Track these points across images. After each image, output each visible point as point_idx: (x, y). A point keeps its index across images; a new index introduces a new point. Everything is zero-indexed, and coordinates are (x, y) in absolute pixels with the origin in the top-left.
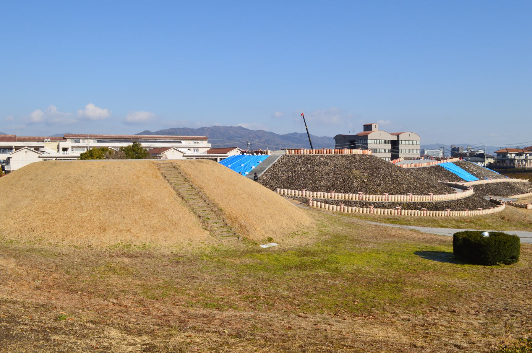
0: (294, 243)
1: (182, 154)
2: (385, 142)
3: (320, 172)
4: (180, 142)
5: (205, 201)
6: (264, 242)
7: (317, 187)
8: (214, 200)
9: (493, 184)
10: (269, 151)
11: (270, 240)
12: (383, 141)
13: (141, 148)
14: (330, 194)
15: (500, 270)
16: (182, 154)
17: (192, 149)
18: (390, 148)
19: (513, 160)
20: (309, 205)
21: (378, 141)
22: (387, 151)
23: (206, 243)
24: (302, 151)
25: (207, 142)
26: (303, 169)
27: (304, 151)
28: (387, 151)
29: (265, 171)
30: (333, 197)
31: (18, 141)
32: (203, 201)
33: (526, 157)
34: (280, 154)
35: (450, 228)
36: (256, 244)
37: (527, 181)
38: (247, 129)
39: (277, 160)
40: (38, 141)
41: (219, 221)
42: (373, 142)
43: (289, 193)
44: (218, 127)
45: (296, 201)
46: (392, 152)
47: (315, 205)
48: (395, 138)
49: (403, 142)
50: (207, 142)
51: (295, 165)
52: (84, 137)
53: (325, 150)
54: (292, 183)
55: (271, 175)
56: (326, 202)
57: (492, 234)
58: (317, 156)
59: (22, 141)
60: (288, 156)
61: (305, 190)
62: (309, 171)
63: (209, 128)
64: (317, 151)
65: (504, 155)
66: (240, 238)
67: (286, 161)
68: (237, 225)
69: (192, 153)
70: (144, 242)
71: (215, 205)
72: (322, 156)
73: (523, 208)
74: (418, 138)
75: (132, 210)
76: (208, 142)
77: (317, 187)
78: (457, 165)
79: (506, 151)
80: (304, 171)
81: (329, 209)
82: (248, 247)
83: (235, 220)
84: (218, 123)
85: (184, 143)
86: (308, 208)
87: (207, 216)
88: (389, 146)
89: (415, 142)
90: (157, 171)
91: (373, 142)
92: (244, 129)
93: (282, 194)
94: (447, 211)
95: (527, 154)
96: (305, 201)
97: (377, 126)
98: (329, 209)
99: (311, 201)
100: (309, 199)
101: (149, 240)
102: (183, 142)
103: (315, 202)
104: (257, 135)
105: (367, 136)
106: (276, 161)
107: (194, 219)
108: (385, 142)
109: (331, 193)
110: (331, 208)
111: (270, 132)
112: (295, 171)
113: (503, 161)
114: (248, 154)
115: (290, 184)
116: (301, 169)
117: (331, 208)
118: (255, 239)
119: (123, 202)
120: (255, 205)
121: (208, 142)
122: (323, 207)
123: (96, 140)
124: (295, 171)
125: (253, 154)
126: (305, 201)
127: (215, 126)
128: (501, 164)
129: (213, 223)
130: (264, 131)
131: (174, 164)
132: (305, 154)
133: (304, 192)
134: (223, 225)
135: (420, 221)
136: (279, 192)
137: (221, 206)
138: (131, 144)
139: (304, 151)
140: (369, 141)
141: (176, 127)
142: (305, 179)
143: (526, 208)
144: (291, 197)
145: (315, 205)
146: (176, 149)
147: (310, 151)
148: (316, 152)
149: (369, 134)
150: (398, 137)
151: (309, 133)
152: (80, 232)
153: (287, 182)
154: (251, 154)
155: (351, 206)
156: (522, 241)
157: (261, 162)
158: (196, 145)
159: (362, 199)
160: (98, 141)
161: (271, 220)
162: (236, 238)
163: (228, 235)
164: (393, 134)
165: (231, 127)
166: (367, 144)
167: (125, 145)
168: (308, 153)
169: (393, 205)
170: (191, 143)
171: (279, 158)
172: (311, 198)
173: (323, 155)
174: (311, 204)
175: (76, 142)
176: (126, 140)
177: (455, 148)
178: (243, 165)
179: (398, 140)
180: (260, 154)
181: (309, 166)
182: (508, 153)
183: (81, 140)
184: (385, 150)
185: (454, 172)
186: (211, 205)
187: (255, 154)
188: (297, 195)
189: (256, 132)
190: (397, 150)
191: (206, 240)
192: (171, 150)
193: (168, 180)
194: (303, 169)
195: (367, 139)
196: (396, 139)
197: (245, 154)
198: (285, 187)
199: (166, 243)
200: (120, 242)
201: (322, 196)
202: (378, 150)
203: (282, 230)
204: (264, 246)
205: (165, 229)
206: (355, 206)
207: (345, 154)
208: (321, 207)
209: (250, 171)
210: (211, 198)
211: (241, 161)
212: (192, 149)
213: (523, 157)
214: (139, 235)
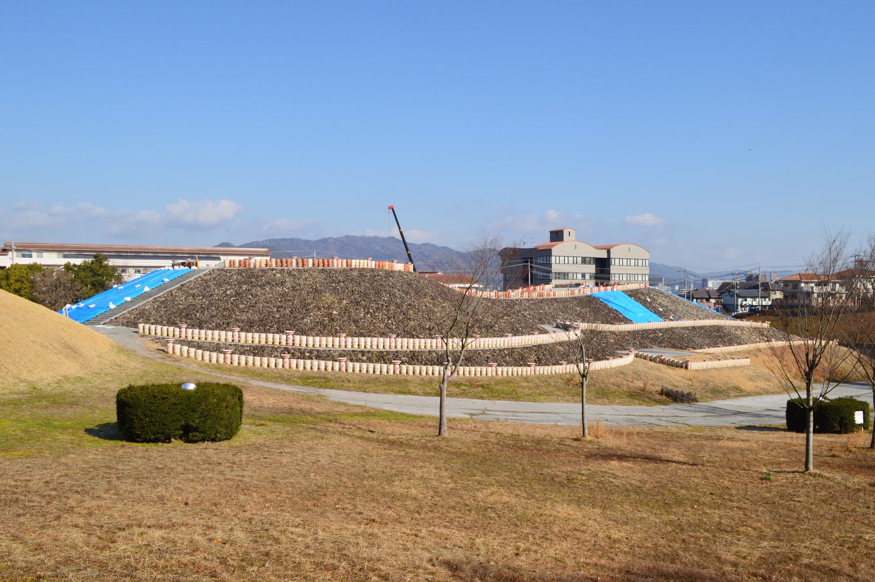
2: (584, 261)
9: (684, 328)
12: (580, 260)
13: (106, 266)
15: (208, 449)
18: (594, 271)
19: (809, 294)
21: (571, 259)
22: (587, 277)
26: (228, 292)
28: (587, 277)
30: (343, 344)
33: (833, 289)
35: (418, 394)
37: (766, 325)
42: (562, 262)
44: (354, 237)
46: (596, 278)
48: (603, 254)
49: (617, 260)
52: (43, 249)
53: (294, 261)
57: (198, 385)
63: (337, 239)
64: (279, 261)
65: (796, 284)
73: (681, 367)
74: (646, 255)
78: (630, 296)
79: (797, 278)
80: (227, 295)
84: (357, 233)
88: (592, 269)
89: (640, 261)
91: (562, 262)
94: (491, 366)
95: (835, 283)
97: (573, 233)
103: (178, 347)
104: (421, 252)
105: (550, 250)
108: (584, 261)
113: (794, 296)
122: (192, 354)
128: (790, 302)
130: (434, 246)
135: (366, 384)
136: (141, 331)
138: (90, 260)
140: (553, 258)
141: (279, 237)
143: (686, 368)
148: (297, 263)
149: (553, 246)
150: (609, 252)
151: (407, 240)
155: (304, 358)
156: (247, 397)
164: (597, 248)
165: (376, 238)
166: (550, 265)
167: (78, 262)
169: (382, 357)
175: (24, 256)
176: (79, 252)
177: (751, 276)
179: (609, 258)
182: (800, 282)
183: (34, 254)
184: (583, 276)
185: (615, 307)
190: (606, 276)
194: (228, 292)
195: (550, 255)
196: (606, 257)
202: (570, 276)
206: (310, 358)
207: (335, 267)
213: (829, 288)
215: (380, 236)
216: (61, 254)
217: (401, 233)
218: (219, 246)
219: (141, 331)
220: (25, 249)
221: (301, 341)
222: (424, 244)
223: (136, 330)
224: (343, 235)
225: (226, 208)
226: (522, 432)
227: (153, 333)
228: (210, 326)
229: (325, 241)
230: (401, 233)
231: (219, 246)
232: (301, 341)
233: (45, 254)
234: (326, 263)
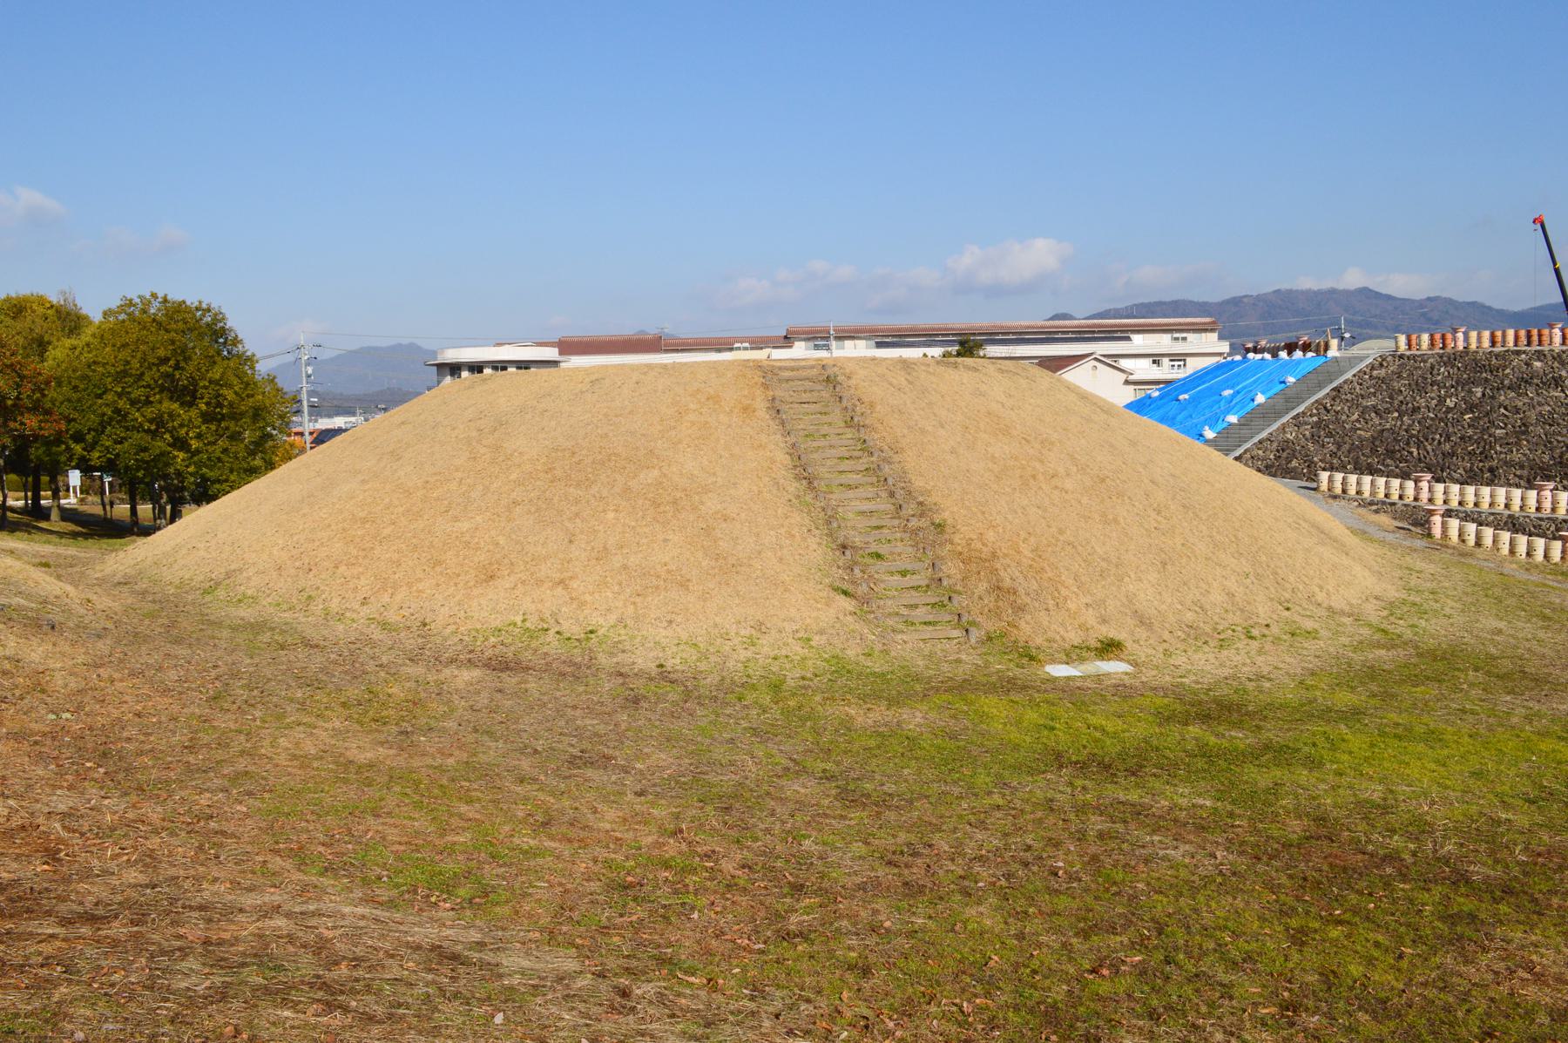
0: (1204, 667)
1: (1123, 377)
3: (1517, 410)
4: (1128, 339)
5: (892, 495)
6: (1072, 655)
7: (1491, 470)
8: (928, 493)
10: (1334, 343)
11: (1109, 648)
14: (1533, 494)
16: (1123, 377)
17: (1166, 361)
20: (1430, 535)
23: (817, 640)
24: (1460, 336)
25: (1215, 335)
26: (1450, 403)
27: (1466, 338)
29: (1301, 409)
30: (1547, 505)
31: (667, 351)
32: (884, 495)
34: (1371, 350)
36: (1032, 658)
38: (1389, 297)
39: (1355, 371)
40: (719, 351)
41: (917, 566)
43: (1366, 489)
45: (1384, 519)
47: (1454, 533)
50: (1215, 335)
51: (1419, 388)
54: (1390, 453)
55: (1317, 425)
56: (1514, 524)
58: (1518, 353)
59: (677, 351)
60: (1401, 357)
61: (1551, 485)
62: (1471, 409)
64: (1523, 333)
66: (975, 634)
67: (1380, 378)
68: (983, 586)
69: (1165, 371)
70: (596, 620)
71: (923, 510)
72: (1540, 355)
75: (611, 515)
76: (1221, 338)
77: (1491, 470)
80: (1449, 410)
81: (1512, 552)
82: (987, 664)
83: (980, 562)
85: (1139, 342)
86: (1420, 543)
87: (874, 548)
90: (759, 392)
92: (1378, 295)
93: (1338, 490)
96: (1417, 520)
98: (1512, 552)
99: (1437, 519)
100: (1431, 513)
101: (612, 619)
102: (1137, 339)
104: (1423, 315)
106: (1349, 375)
107: (817, 550)
109: (1540, 489)
110: (1522, 549)
111: (1473, 304)
112: (1416, 410)
114: (1259, 356)
115: (1384, 454)
116: (1441, 401)
117: (1522, 549)
118: (1039, 641)
119: (594, 490)
120: (1104, 515)
121: (1221, 338)
122: (1488, 541)
123: (872, 343)
124: (1416, 410)
125: (1275, 355)
126: (1417, 520)
127: (1278, 292)
129: (892, 574)
130: (1450, 301)
131: (830, 372)
132: (1473, 346)
133: (1547, 494)
134: (924, 583)
136: (1324, 486)
137: (946, 515)
139: (1466, 338)
142: (1448, 439)
144: (1371, 504)
145: (1454, 533)
146: (1111, 361)
147: (1493, 336)
152: (420, 580)
153: (1374, 451)
154: (1267, 356)
157: (1291, 380)
158: (1180, 348)
159: (1554, 510)
160: (880, 345)
161: (1153, 576)
162: (956, 633)
163: (930, 618)
165: (1333, 291)
168: (1486, 343)
170: (1163, 343)
171: (1362, 365)
172: (1439, 504)
173: (1546, 348)
174: (1437, 531)
175: (817, 347)
178: (1227, 393)
180: (1298, 354)
181: (1478, 391)
186: (909, 509)
187: (1283, 354)
188: (1395, 497)
189: (1421, 304)
191: (821, 632)
192: (1088, 365)
193: (783, 423)
194: (1450, 403)
197: (1251, 355)
198: (1360, 469)
199: (669, 633)
200: (518, 619)
201: (1501, 500)
203: (1190, 616)
204: (1059, 671)
205: (684, 585)
208: (1478, 544)
209: (1242, 413)
210: (918, 483)
211: (1227, 380)
212: (1166, 361)
214: (588, 598)
215: (1341, 286)
216: (811, 344)
217: (1557, 272)
218: (1052, 319)
219: (1324, 486)
220: (818, 337)
221: (1509, 498)
222: (1429, 299)
223: (1314, 485)
224: (1270, 289)
225: (1038, 255)
226: (26, 535)
227: (1352, 491)
228: (1456, 476)
229: (1236, 302)
230: (1557, 272)
231: (1052, 319)
232: (1509, 498)
233: (848, 343)
234: (1535, 338)
